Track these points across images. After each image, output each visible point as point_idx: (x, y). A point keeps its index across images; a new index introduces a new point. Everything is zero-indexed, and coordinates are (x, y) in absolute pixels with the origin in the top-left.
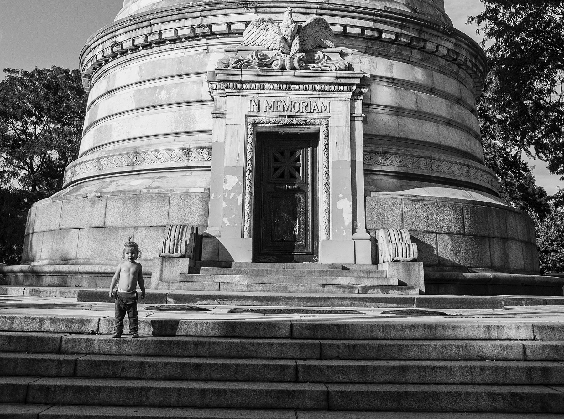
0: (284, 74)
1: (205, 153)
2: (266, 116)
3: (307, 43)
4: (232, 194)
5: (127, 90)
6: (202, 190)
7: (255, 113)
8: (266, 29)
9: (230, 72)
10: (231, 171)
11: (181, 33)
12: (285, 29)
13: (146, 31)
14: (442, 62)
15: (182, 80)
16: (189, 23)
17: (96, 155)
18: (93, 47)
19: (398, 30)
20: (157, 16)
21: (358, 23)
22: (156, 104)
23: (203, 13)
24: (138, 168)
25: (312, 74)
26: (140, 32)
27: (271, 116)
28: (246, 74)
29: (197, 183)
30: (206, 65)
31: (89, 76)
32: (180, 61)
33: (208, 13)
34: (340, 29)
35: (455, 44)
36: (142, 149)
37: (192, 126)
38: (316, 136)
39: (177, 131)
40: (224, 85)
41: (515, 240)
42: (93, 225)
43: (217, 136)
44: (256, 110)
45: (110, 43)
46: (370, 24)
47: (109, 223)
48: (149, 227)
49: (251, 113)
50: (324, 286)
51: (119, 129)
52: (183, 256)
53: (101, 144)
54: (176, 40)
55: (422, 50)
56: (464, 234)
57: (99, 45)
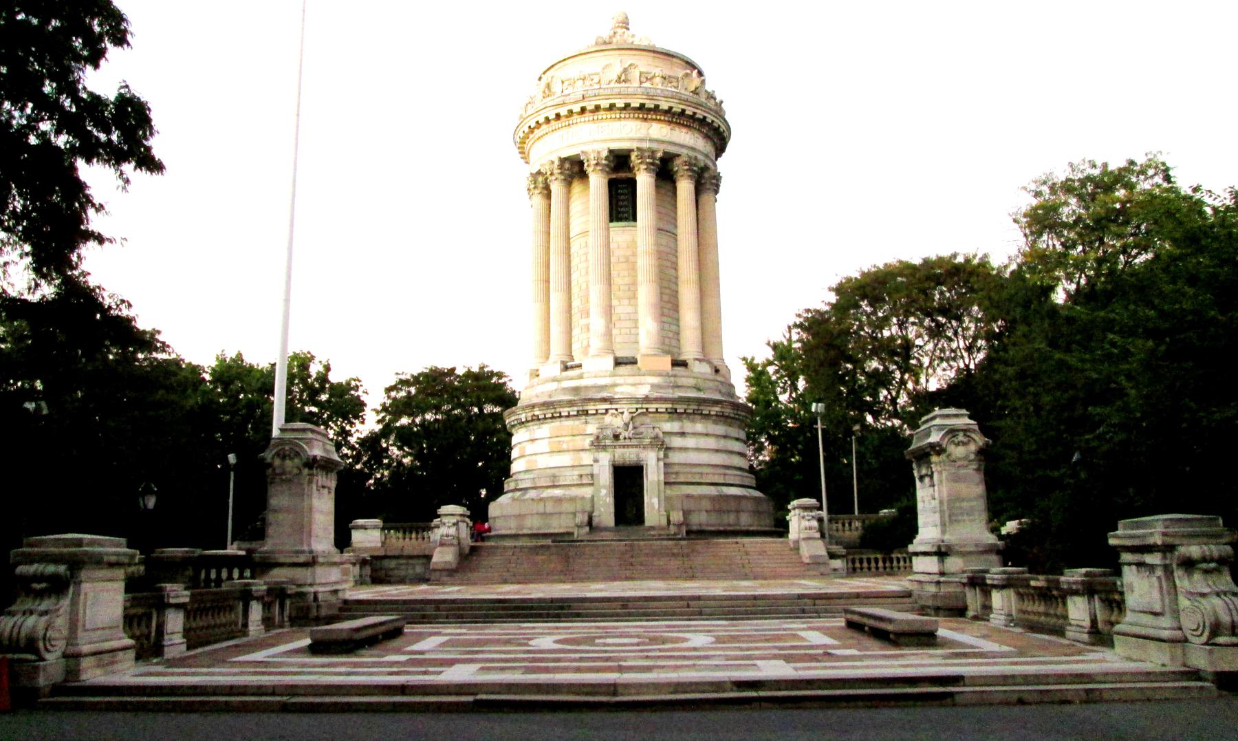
10: (604, 487)
28: (608, 442)
29: (587, 492)
54: (568, 416)
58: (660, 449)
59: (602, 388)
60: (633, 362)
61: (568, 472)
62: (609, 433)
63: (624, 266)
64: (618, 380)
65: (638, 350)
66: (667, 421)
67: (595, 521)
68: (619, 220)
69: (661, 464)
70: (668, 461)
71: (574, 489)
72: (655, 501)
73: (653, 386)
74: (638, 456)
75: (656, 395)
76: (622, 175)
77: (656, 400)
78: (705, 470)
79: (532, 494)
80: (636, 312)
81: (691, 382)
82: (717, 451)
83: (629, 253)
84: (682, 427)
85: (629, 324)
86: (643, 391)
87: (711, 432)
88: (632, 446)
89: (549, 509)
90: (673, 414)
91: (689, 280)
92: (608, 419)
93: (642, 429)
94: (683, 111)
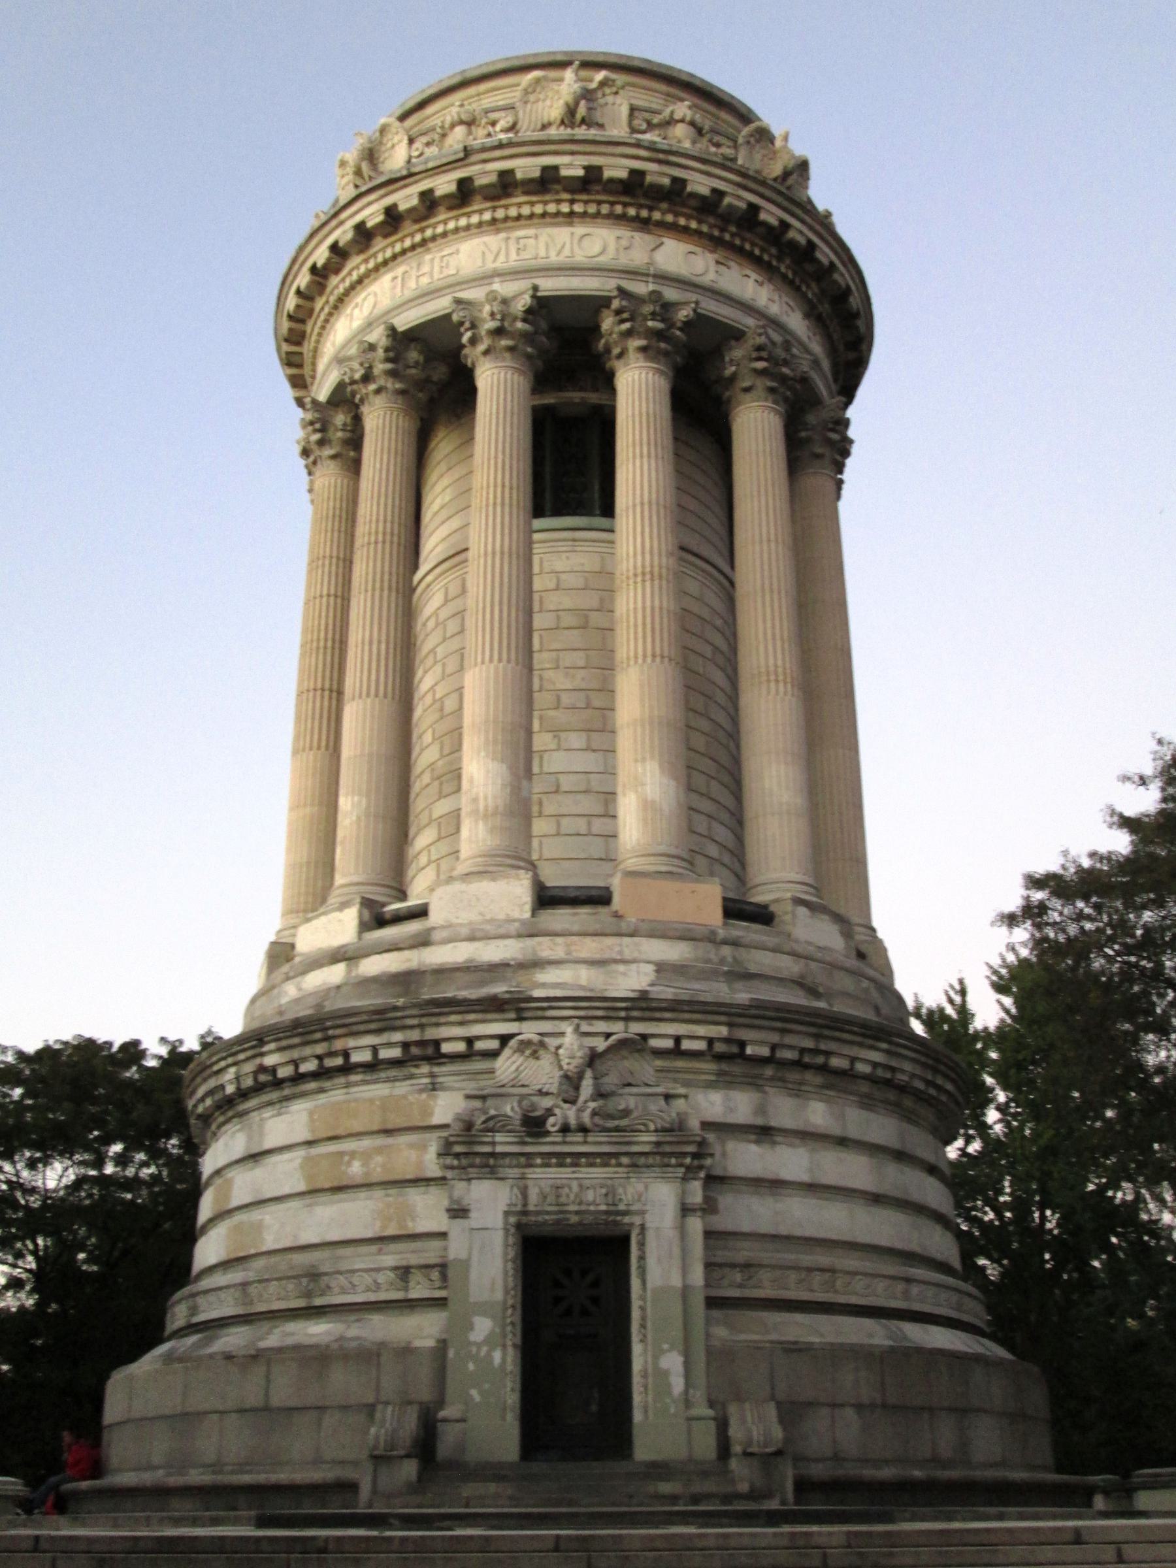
0: (568, 1139)
1: (435, 1275)
2: (538, 1213)
3: (606, 1080)
4: (484, 1349)
5: (287, 1156)
6: (431, 1343)
7: (519, 1208)
8: (535, 1055)
9: (474, 1139)
11: (384, 1054)
12: (567, 1061)
13: (320, 1049)
14: (865, 1088)
15: (390, 1141)
16: (398, 1037)
17: (235, 1276)
18: (215, 1068)
19: (775, 1038)
20: (339, 1022)
21: (701, 1030)
22: (345, 1183)
23: (424, 1020)
24: (318, 1302)
25: (614, 1139)
26: (308, 1051)
27: (548, 1213)
28: (503, 1142)
29: (422, 1330)
30: (431, 1114)
31: (206, 1119)
32: (385, 1105)
33: (434, 1020)
34: (669, 1044)
35: (888, 1052)
36: (323, 1269)
37: (410, 1224)
38: (625, 1240)
39: (386, 1234)
40: (464, 1162)
41: (985, 1411)
42: (248, 1406)
43: (456, 1249)
44: (520, 1203)
45: (249, 1067)
46: (724, 1031)
47: (276, 1401)
48: (345, 1408)
49: (513, 1209)
50: (631, 1497)
51: (278, 1229)
52: (408, 1456)
53: (242, 1254)
54: (372, 1066)
55: (824, 1069)
56: (884, 1406)
57: (228, 1066)
58: (690, 1173)
59: (496, 969)
60: (599, 898)
61: (362, 1259)
62: (510, 1108)
63: (574, 638)
64: (546, 948)
65: (609, 859)
66: (710, 1086)
67: (445, 1448)
68: (557, 512)
69: (696, 1225)
70: (722, 1222)
71: (376, 1319)
72: (673, 1362)
73: (661, 968)
74: (610, 1193)
75: (666, 992)
76: (576, 397)
77: (677, 1008)
78: (851, 1262)
79: (234, 1339)
80: (610, 772)
81: (788, 966)
82: (877, 1199)
83: (591, 600)
84: (761, 1110)
85: (588, 804)
86: (630, 981)
87: (853, 1132)
88: (591, 1159)
89: (283, 1392)
90: (731, 1062)
91: (763, 697)
92: (507, 1065)
93: (628, 1100)
94: (754, 209)
